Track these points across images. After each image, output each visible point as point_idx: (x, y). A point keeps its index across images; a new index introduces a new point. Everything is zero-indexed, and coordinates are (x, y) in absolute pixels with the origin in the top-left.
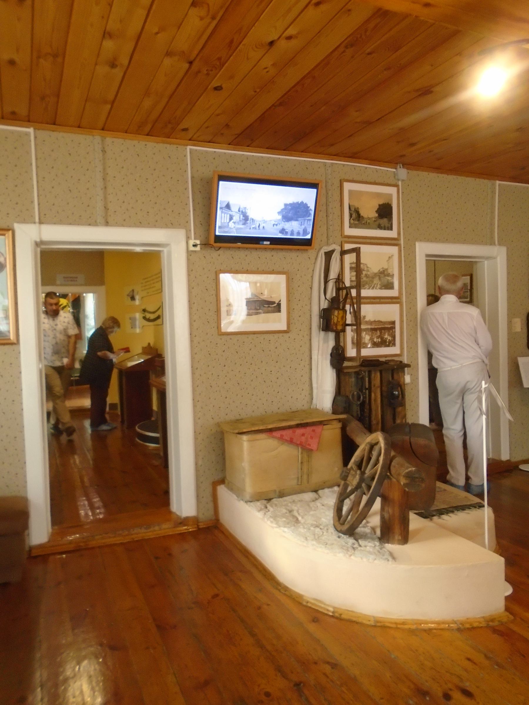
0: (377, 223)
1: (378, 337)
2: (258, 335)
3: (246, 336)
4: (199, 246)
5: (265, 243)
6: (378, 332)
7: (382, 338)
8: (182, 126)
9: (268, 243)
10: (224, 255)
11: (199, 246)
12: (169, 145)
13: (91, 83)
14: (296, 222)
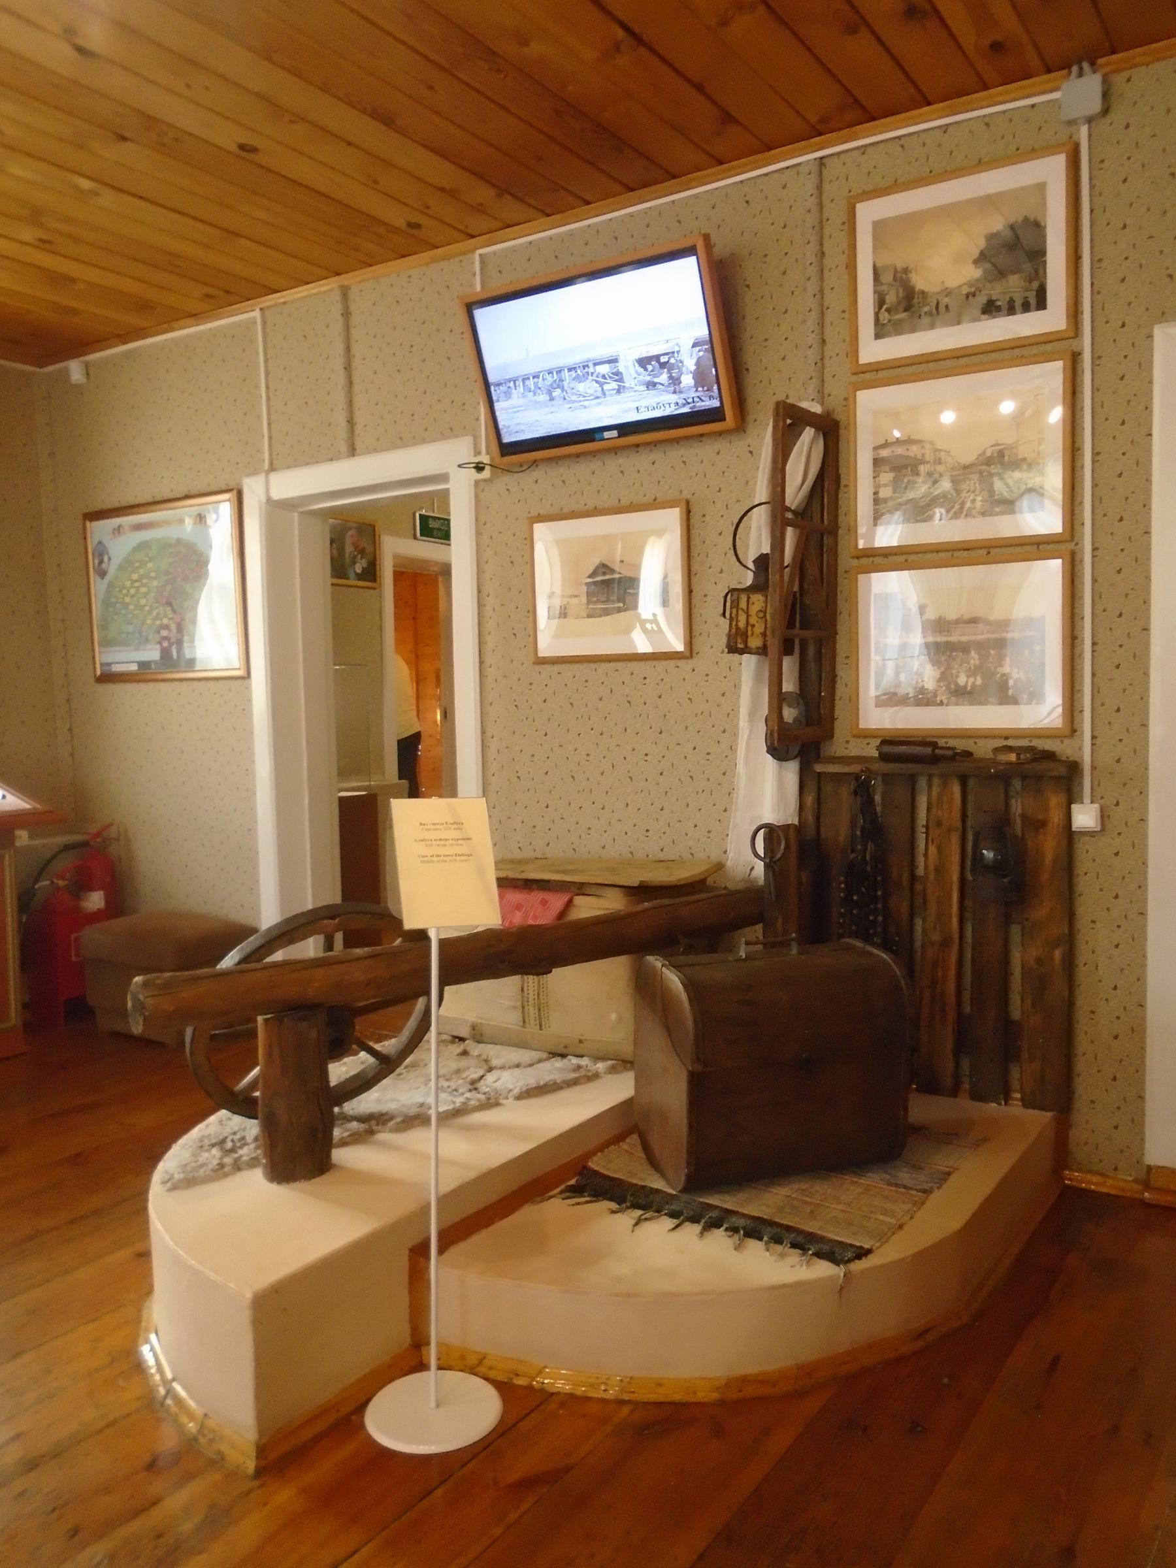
0: (982, 299)
1: (972, 673)
2: (619, 665)
3: (593, 665)
4: (488, 468)
5: (607, 435)
6: (973, 653)
7: (988, 675)
8: (347, 560)
9: (615, 433)
10: (544, 482)
11: (488, 468)
12: (446, 262)
13: (320, 162)
14: (1016, 276)
